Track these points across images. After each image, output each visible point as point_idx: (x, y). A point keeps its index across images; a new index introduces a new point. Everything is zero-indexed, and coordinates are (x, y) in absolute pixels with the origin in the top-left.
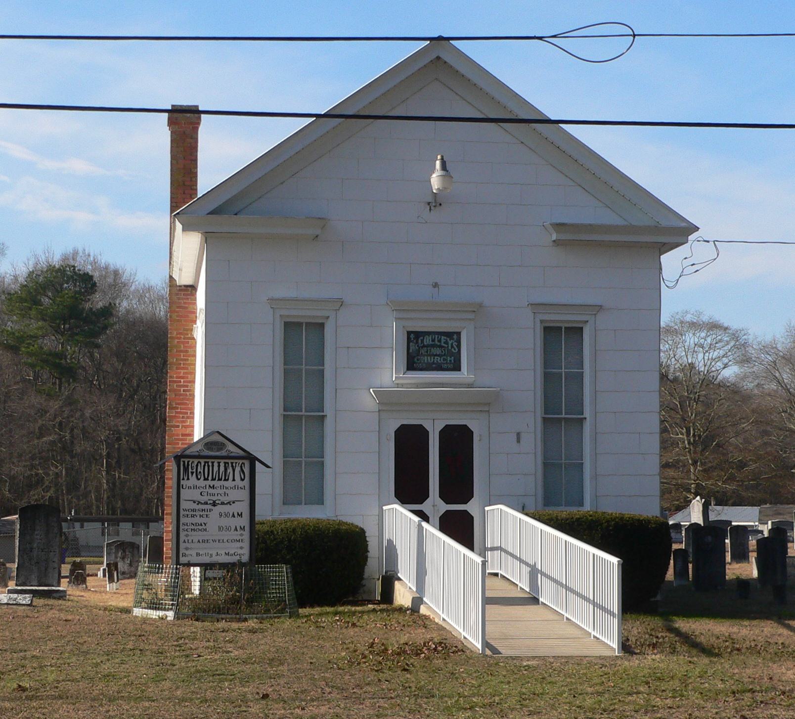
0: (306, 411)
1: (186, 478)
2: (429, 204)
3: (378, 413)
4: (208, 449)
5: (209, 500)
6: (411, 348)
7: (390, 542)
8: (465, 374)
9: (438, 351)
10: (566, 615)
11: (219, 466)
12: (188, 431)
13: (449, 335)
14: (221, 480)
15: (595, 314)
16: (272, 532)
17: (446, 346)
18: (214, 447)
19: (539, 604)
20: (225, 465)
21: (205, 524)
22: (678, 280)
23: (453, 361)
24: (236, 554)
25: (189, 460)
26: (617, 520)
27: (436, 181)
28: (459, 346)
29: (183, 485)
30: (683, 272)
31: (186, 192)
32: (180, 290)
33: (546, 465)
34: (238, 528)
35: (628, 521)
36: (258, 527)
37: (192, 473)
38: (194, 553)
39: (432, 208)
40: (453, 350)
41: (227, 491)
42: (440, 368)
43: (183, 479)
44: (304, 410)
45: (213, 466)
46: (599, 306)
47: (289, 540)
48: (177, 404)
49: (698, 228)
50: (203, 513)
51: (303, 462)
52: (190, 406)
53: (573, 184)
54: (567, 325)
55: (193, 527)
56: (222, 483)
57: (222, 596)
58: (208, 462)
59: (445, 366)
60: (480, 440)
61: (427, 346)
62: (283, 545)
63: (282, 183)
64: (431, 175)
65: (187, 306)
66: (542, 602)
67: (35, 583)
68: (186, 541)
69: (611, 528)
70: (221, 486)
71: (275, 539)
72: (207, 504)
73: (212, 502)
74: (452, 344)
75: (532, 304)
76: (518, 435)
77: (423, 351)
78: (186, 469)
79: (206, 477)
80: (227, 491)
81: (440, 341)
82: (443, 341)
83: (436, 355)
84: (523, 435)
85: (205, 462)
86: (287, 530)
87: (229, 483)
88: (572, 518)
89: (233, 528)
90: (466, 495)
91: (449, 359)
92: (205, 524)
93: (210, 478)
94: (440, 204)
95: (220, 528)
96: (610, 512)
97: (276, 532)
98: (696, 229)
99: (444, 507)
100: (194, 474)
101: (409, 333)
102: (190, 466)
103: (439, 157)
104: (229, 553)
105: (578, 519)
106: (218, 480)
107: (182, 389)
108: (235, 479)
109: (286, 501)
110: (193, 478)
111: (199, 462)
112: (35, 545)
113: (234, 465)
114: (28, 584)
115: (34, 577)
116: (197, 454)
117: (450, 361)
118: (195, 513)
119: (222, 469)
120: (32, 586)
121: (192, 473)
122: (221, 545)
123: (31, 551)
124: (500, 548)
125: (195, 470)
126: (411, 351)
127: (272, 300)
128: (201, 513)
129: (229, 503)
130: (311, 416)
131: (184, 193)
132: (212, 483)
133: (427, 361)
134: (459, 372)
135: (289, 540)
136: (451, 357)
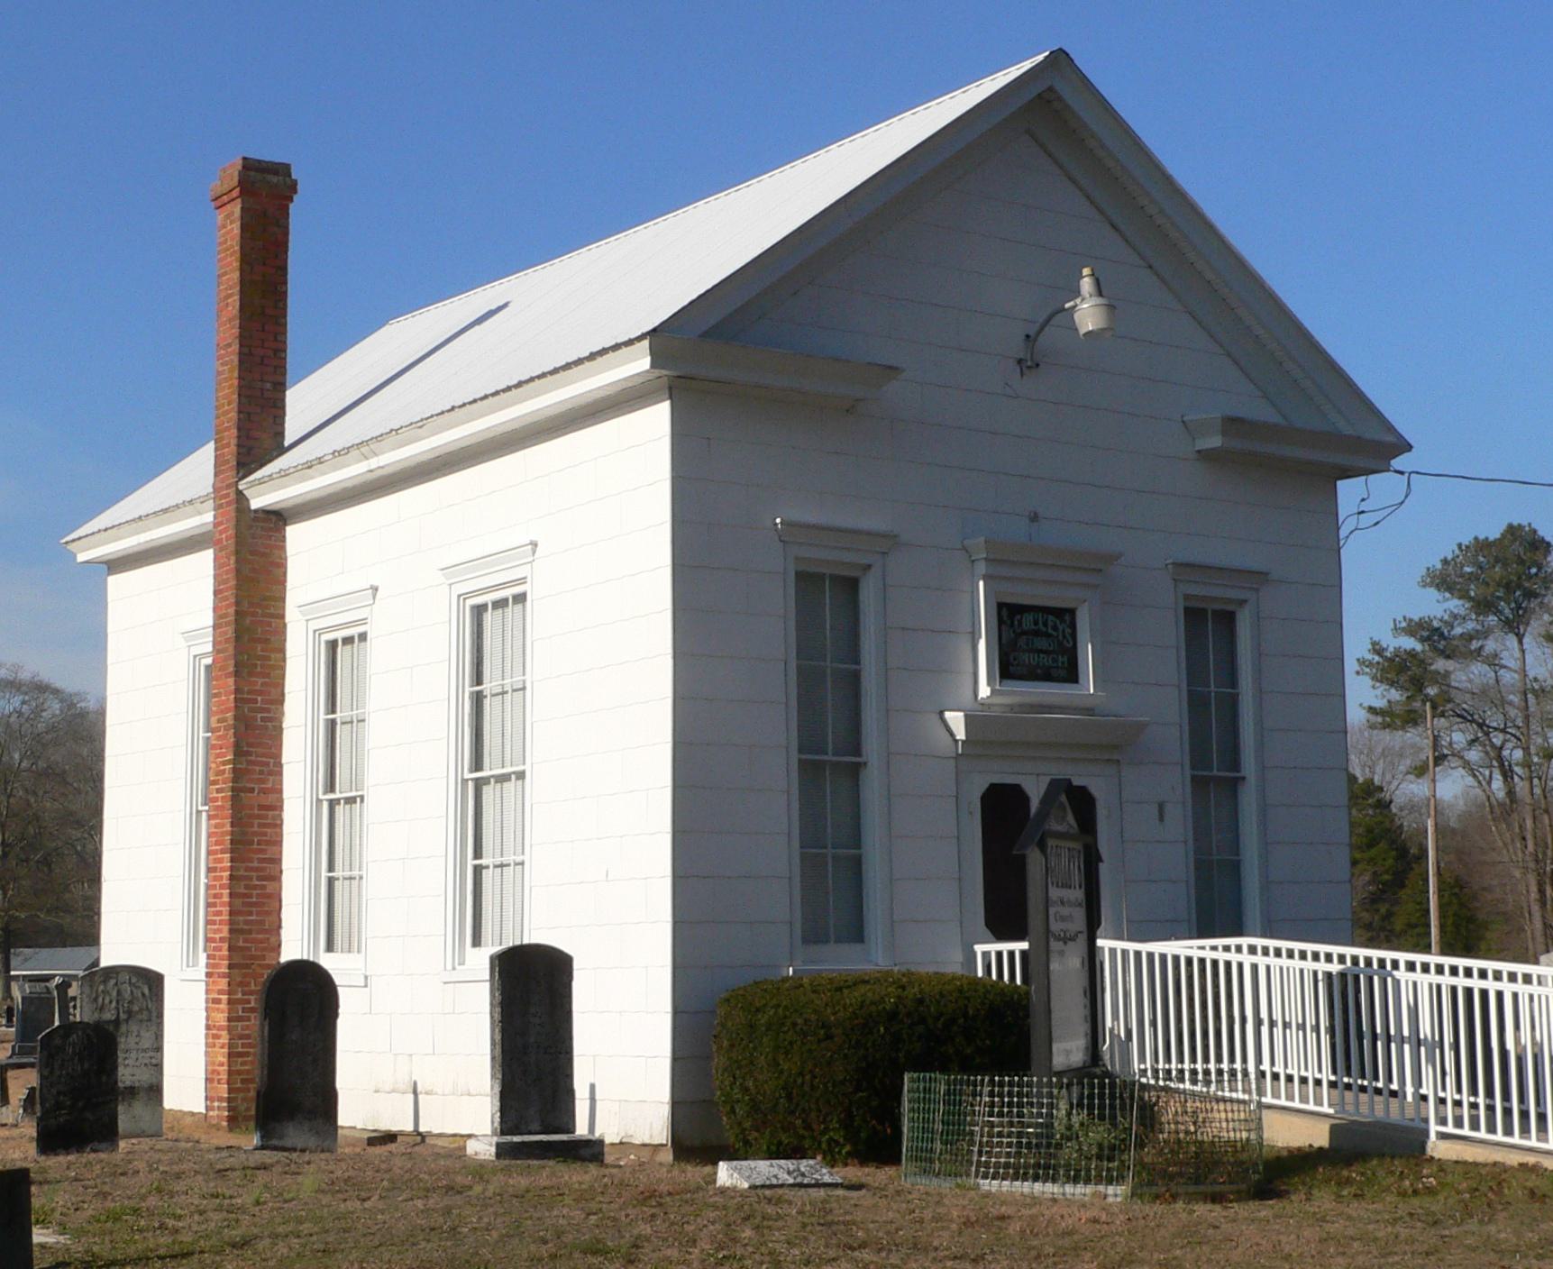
2: (1020, 362)
9: (1041, 643)
12: (271, 799)
17: (1055, 634)
31: (266, 327)
32: (256, 519)
40: (1065, 642)
42: (1047, 676)
44: (830, 753)
52: (273, 750)
54: (1218, 606)
65: (268, 551)
67: (536, 1126)
74: (1063, 631)
77: (1022, 641)
81: (1045, 624)
82: (1050, 623)
83: (1041, 651)
84: (1168, 808)
91: (1060, 659)
94: (1038, 365)
98: (1409, 447)
103: (1086, 271)
109: (814, 934)
112: (532, 1040)
117: (1063, 663)
131: (263, 331)
134: (1075, 685)
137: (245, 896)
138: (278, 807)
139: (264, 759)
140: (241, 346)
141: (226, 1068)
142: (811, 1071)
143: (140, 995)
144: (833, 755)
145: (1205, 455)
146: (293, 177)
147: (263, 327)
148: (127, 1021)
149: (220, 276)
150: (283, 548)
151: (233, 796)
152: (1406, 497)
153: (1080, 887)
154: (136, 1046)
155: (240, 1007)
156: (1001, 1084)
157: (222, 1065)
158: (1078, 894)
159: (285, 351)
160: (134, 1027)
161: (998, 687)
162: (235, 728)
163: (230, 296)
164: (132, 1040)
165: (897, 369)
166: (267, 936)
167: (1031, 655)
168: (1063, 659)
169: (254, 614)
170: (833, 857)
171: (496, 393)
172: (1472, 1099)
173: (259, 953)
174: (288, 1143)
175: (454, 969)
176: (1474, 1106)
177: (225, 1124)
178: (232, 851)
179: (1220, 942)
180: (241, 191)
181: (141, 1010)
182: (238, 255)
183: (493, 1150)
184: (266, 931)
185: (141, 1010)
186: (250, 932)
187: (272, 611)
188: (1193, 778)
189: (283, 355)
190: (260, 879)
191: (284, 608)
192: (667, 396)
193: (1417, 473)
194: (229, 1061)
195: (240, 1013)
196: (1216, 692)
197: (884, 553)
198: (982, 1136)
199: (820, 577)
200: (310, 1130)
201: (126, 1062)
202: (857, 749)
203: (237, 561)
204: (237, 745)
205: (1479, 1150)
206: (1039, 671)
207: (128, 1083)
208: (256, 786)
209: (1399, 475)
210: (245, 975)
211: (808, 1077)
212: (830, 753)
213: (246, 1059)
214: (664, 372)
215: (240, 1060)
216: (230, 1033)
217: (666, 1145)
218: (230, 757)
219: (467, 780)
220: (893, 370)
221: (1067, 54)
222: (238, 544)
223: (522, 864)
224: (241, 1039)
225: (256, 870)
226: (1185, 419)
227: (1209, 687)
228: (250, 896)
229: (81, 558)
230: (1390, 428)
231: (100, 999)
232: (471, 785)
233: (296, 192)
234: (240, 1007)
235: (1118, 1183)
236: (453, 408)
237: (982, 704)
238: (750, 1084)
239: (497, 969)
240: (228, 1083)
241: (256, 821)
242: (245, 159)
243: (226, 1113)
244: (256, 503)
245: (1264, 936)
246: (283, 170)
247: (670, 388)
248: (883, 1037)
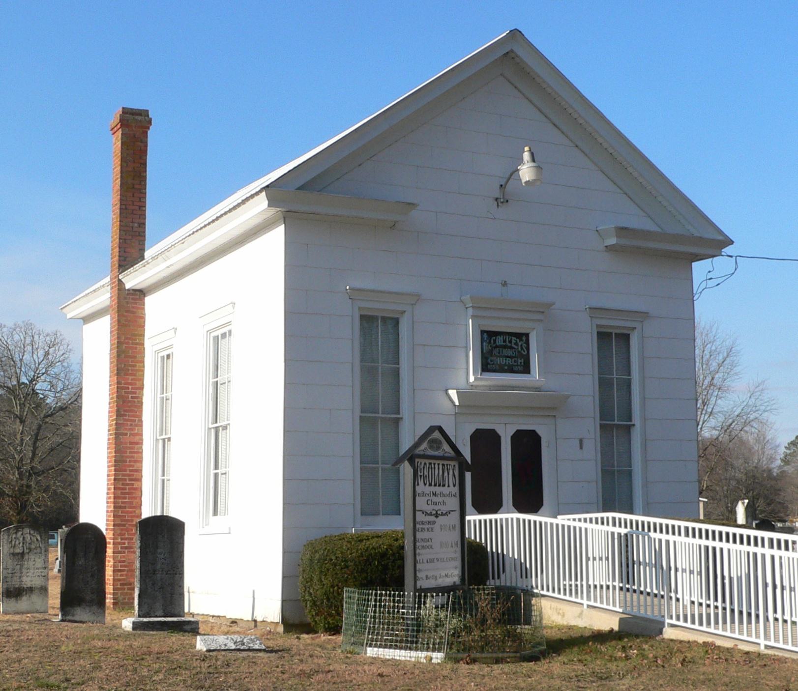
2: (497, 199)
9: (509, 352)
12: (136, 439)
13: (519, 336)
17: (516, 347)
23: (523, 364)
28: (528, 349)
31: (135, 195)
32: (128, 294)
39: (500, 204)
40: (522, 352)
42: (511, 370)
44: (380, 412)
48: (125, 411)
52: (138, 413)
53: (622, 192)
54: (618, 331)
59: (516, 368)
61: (501, 346)
63: (360, 165)
67: (160, 613)
74: (521, 345)
76: (581, 441)
77: (496, 351)
81: (510, 342)
82: (513, 342)
83: (508, 357)
84: (585, 442)
94: (507, 201)
98: (732, 242)
101: (483, 332)
103: (526, 149)
107: (130, 396)
109: (368, 510)
112: (159, 566)
114: (152, 614)
115: (159, 606)
117: (521, 363)
120: (156, 616)
123: (154, 574)
131: (133, 196)
137: (123, 489)
138: (140, 443)
139: (132, 418)
140: (121, 205)
141: (112, 577)
142: (337, 585)
144: (382, 414)
145: (609, 248)
146: (150, 116)
147: (133, 195)
148: (28, 553)
149: (113, 169)
150: (143, 309)
151: (116, 437)
152: (736, 269)
153: (454, 486)
155: (120, 546)
156: (381, 595)
157: (111, 576)
158: (456, 490)
159: (145, 207)
160: (32, 557)
161: (479, 376)
162: (117, 402)
163: (117, 179)
164: (31, 563)
165: (413, 204)
166: (134, 510)
167: (501, 359)
168: (521, 361)
169: (128, 343)
170: (382, 469)
171: (209, 224)
172: (715, 604)
173: (130, 519)
174: (77, 618)
175: (203, 527)
176: (716, 607)
177: (112, 606)
178: (115, 466)
179: (577, 516)
180: (121, 125)
181: (36, 548)
182: (120, 158)
183: (131, 625)
184: (134, 507)
185: (36, 548)
186: (125, 507)
187: (137, 341)
188: (601, 425)
189: (144, 209)
190: (130, 480)
191: (144, 340)
192: (283, 222)
193: (740, 256)
194: (113, 574)
195: (120, 549)
197: (412, 304)
198: (370, 623)
199: (609, 335)
200: (90, 612)
201: (28, 574)
202: (630, 419)
203: (118, 316)
204: (118, 411)
205: (686, 634)
207: (29, 585)
208: (129, 433)
209: (730, 258)
210: (122, 530)
211: (336, 588)
212: (380, 412)
213: (122, 573)
214: (279, 209)
215: (119, 573)
216: (114, 560)
217: (279, 623)
218: (115, 417)
219: (211, 428)
220: (412, 205)
221: (520, 32)
222: (118, 307)
223: (225, 474)
224: (119, 562)
225: (129, 475)
226: (598, 229)
227: (613, 375)
228: (125, 489)
229: (69, 316)
230: (720, 232)
231: (13, 543)
232: (213, 431)
233: (151, 125)
234: (120, 546)
235: (439, 651)
236: (193, 233)
237: (472, 386)
238: (311, 591)
239: (138, 529)
240: (113, 585)
241: (128, 451)
242: (123, 108)
243: (112, 601)
244: (128, 286)
245: (644, 515)
246: (144, 113)
247: (284, 218)
248: (377, 567)
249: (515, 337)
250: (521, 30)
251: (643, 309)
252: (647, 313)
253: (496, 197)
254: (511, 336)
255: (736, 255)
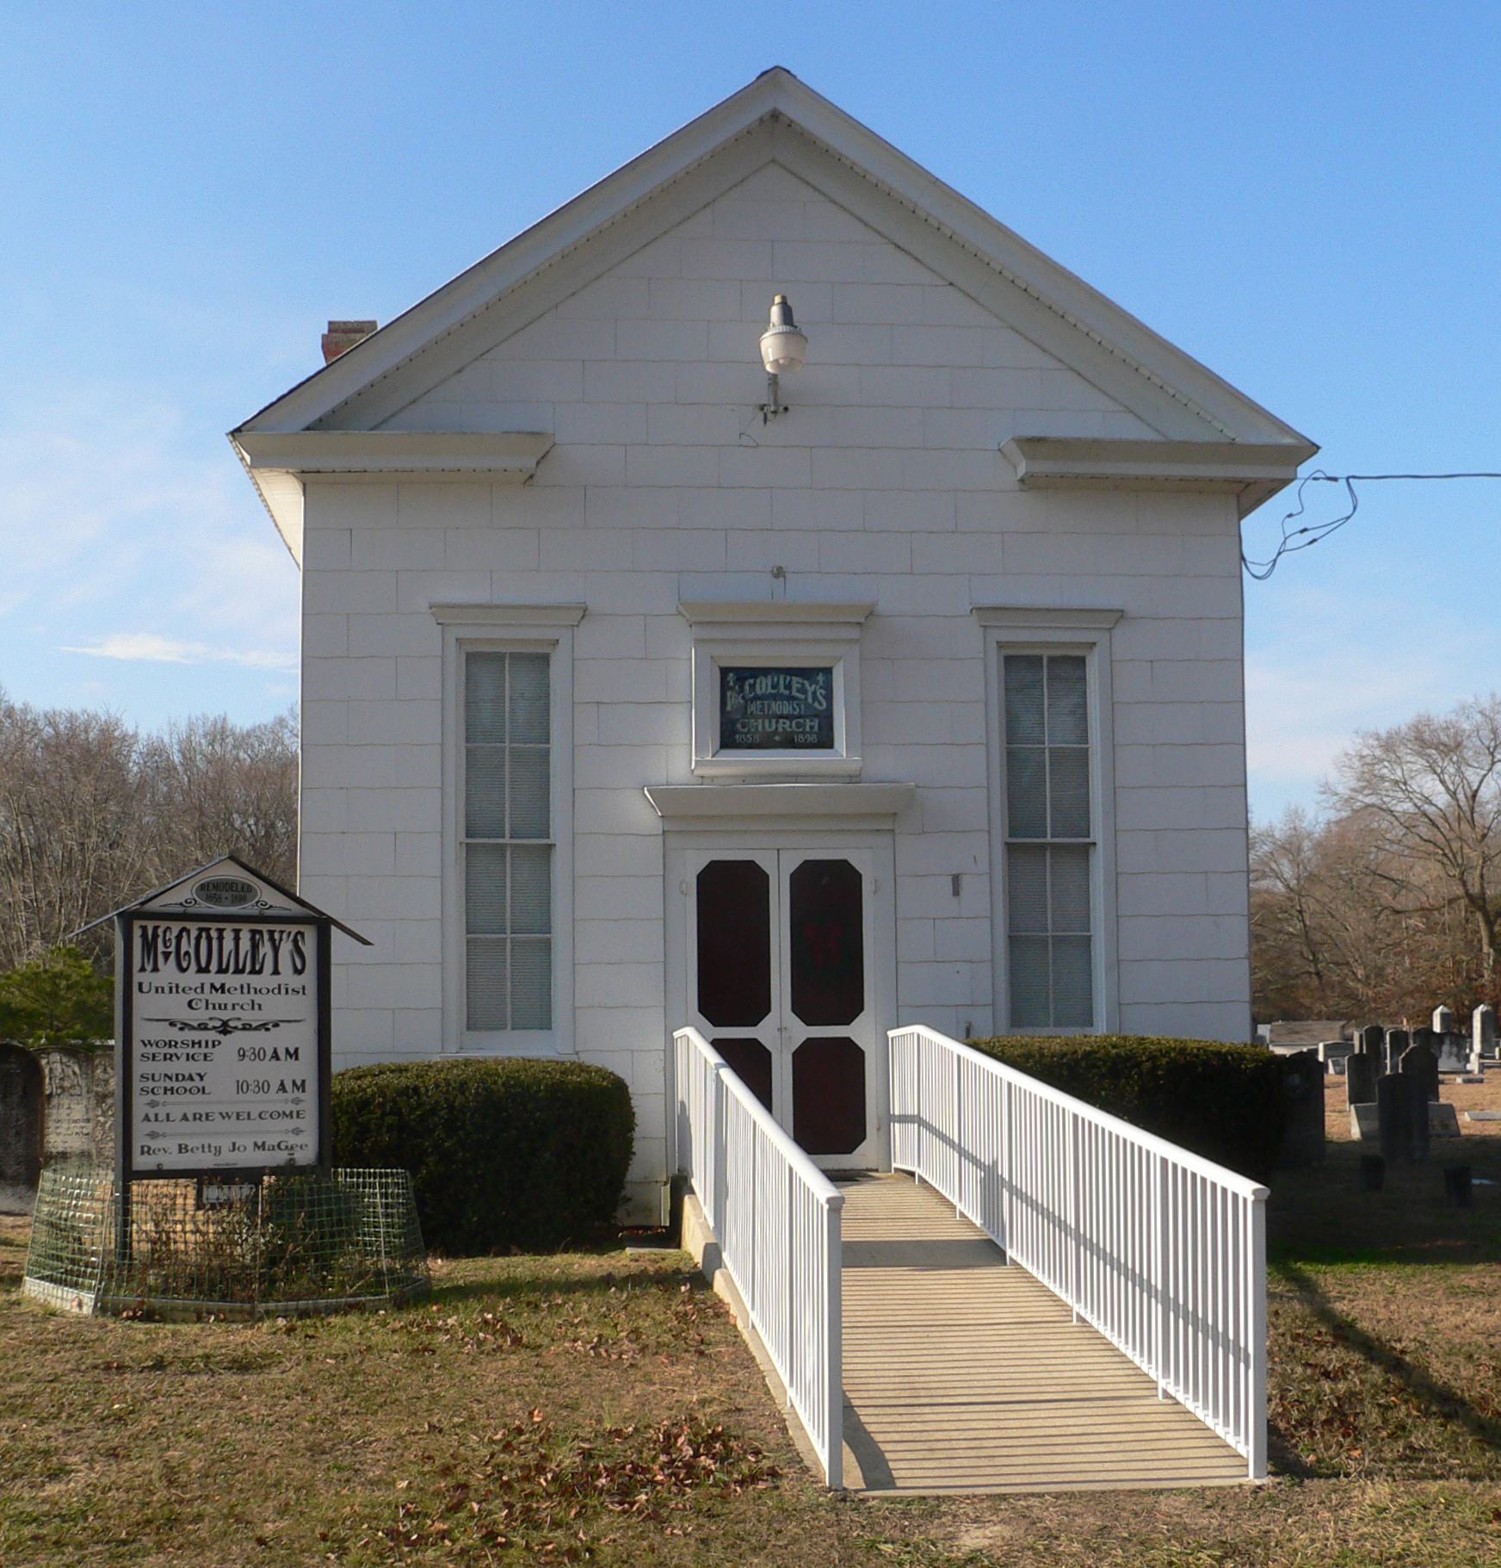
0: (511, 837)
1: (149, 967)
3: (661, 838)
4: (209, 899)
5: (211, 1019)
6: (729, 703)
7: (682, 1103)
8: (842, 754)
9: (786, 708)
10: (1078, 1308)
11: (237, 939)
13: (807, 673)
14: (242, 971)
15: (1110, 629)
16: (416, 1089)
17: (803, 697)
18: (224, 894)
19: (1005, 1264)
20: (253, 939)
21: (202, 1078)
22: (1275, 561)
23: (816, 729)
24: (283, 1146)
25: (157, 923)
26: (1173, 1055)
27: (770, 347)
28: (829, 698)
29: (140, 985)
30: (1284, 542)
33: (1013, 941)
34: (289, 1086)
35: (1197, 1056)
36: (336, 1087)
37: (167, 955)
38: (172, 1144)
39: (770, 416)
40: (816, 704)
41: (258, 999)
42: (790, 742)
43: (143, 969)
45: (221, 939)
46: (1118, 611)
47: (451, 1107)
49: (1318, 448)
50: (196, 1049)
51: (508, 941)
55: (169, 1084)
56: (245, 978)
57: (249, 1246)
58: (208, 930)
59: (800, 739)
60: (875, 892)
62: (436, 1119)
63: (459, 371)
64: (763, 334)
66: (1011, 1259)
68: (152, 1117)
69: (1160, 1072)
70: (242, 987)
71: (420, 1105)
72: (206, 1028)
73: (218, 1024)
74: (814, 693)
75: (980, 609)
76: (956, 879)
77: (752, 708)
78: (149, 946)
79: (203, 964)
80: (258, 999)
81: (788, 687)
82: (795, 686)
83: (781, 717)
84: (965, 882)
85: (201, 930)
86: (448, 1084)
87: (265, 980)
88: (1076, 1052)
89: (275, 1085)
90: (850, 1008)
92: (202, 1078)
93: (214, 966)
94: (786, 409)
95: (241, 1087)
96: (1154, 1037)
97: (423, 1090)
98: (1314, 449)
99: (802, 1032)
100: (172, 957)
101: (724, 672)
102: (160, 940)
103: (777, 299)
104: (264, 1143)
105: (1087, 1055)
106: (234, 972)
108: (280, 969)
110: (168, 971)
111: (183, 929)
113: (277, 936)
116: (180, 909)
117: (811, 727)
118: (172, 1051)
119: (245, 945)
121: (167, 955)
122: (245, 1125)
124: (917, 1120)
125: (172, 949)
126: (729, 708)
127: (438, 608)
128: (191, 1051)
129: (264, 1027)
130: (524, 846)
132: (218, 979)
133: (763, 727)
135: (451, 1107)
136: (811, 721)
143: (71, 1073)
148: (59, 1095)
152: (1355, 508)
154: (67, 1118)
160: (65, 1101)
164: (63, 1113)
181: (73, 1086)
185: (73, 1086)
196: (1050, 749)
199: (1034, 662)
200: (13, 1195)
201: (58, 1131)
206: (777, 738)
207: (60, 1149)
221: (788, 72)
242: (330, 323)
249: (797, 676)
250: (787, 68)
251: (1116, 605)
252: (1122, 611)
253: (763, 402)
254: (791, 675)
255: (1345, 476)
